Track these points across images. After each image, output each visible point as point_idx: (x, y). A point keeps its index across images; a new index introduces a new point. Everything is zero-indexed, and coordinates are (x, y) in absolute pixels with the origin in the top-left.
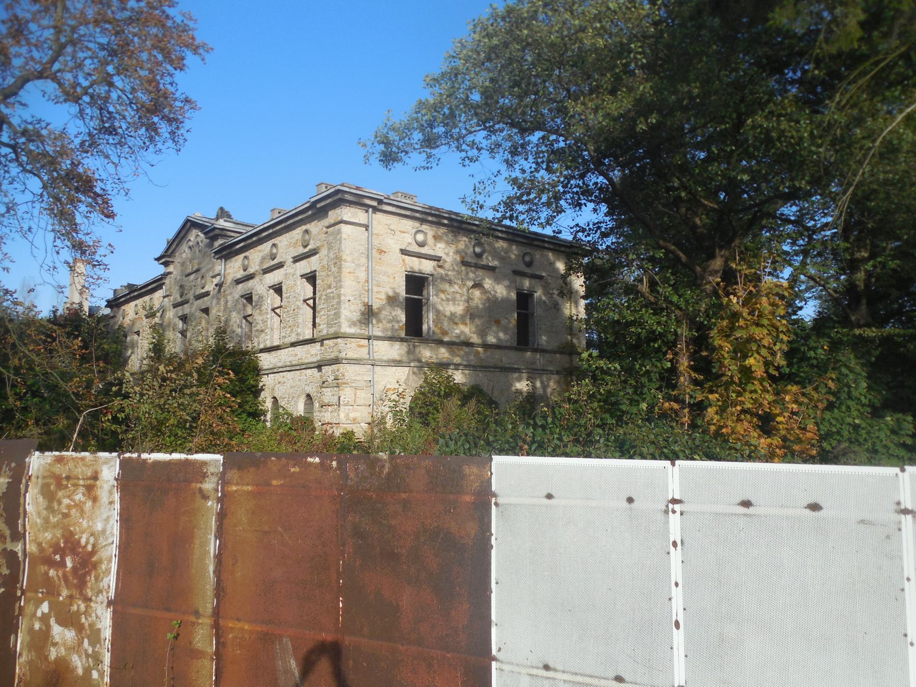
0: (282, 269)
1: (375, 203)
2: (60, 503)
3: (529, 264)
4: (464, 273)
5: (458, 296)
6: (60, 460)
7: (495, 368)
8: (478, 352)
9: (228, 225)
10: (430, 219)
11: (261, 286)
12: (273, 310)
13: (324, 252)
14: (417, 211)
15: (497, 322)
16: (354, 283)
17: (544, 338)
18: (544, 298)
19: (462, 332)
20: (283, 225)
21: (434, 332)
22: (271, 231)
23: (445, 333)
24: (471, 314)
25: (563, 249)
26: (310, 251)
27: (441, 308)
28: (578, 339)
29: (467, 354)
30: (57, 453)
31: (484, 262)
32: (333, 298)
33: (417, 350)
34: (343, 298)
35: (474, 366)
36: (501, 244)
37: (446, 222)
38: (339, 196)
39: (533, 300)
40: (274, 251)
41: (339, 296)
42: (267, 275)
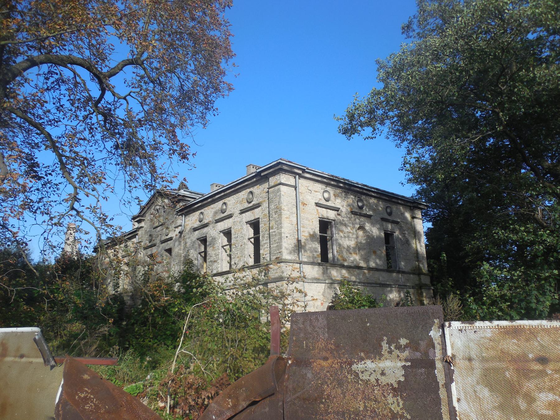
0: (231, 219)
1: (300, 172)
2: (530, 399)
3: (390, 214)
4: (353, 219)
5: (351, 235)
6: (516, 332)
7: (377, 284)
8: (365, 273)
9: (187, 194)
10: (332, 183)
11: (214, 232)
12: (223, 247)
13: (265, 205)
14: (325, 178)
15: (375, 252)
16: (289, 225)
17: (403, 263)
18: (400, 236)
19: (355, 260)
20: (233, 189)
21: (338, 259)
22: (223, 194)
23: (345, 260)
24: (359, 247)
25: (409, 204)
26: (254, 205)
27: (342, 243)
28: (422, 264)
29: (358, 274)
30: (504, 323)
31: (364, 212)
32: (275, 235)
33: (328, 271)
34: (283, 235)
35: (364, 283)
36: (373, 201)
37: (341, 185)
38: (280, 167)
39: (393, 238)
40: (224, 207)
41: (280, 234)
42: (219, 224)
